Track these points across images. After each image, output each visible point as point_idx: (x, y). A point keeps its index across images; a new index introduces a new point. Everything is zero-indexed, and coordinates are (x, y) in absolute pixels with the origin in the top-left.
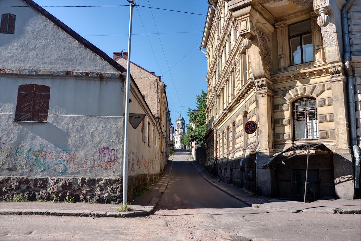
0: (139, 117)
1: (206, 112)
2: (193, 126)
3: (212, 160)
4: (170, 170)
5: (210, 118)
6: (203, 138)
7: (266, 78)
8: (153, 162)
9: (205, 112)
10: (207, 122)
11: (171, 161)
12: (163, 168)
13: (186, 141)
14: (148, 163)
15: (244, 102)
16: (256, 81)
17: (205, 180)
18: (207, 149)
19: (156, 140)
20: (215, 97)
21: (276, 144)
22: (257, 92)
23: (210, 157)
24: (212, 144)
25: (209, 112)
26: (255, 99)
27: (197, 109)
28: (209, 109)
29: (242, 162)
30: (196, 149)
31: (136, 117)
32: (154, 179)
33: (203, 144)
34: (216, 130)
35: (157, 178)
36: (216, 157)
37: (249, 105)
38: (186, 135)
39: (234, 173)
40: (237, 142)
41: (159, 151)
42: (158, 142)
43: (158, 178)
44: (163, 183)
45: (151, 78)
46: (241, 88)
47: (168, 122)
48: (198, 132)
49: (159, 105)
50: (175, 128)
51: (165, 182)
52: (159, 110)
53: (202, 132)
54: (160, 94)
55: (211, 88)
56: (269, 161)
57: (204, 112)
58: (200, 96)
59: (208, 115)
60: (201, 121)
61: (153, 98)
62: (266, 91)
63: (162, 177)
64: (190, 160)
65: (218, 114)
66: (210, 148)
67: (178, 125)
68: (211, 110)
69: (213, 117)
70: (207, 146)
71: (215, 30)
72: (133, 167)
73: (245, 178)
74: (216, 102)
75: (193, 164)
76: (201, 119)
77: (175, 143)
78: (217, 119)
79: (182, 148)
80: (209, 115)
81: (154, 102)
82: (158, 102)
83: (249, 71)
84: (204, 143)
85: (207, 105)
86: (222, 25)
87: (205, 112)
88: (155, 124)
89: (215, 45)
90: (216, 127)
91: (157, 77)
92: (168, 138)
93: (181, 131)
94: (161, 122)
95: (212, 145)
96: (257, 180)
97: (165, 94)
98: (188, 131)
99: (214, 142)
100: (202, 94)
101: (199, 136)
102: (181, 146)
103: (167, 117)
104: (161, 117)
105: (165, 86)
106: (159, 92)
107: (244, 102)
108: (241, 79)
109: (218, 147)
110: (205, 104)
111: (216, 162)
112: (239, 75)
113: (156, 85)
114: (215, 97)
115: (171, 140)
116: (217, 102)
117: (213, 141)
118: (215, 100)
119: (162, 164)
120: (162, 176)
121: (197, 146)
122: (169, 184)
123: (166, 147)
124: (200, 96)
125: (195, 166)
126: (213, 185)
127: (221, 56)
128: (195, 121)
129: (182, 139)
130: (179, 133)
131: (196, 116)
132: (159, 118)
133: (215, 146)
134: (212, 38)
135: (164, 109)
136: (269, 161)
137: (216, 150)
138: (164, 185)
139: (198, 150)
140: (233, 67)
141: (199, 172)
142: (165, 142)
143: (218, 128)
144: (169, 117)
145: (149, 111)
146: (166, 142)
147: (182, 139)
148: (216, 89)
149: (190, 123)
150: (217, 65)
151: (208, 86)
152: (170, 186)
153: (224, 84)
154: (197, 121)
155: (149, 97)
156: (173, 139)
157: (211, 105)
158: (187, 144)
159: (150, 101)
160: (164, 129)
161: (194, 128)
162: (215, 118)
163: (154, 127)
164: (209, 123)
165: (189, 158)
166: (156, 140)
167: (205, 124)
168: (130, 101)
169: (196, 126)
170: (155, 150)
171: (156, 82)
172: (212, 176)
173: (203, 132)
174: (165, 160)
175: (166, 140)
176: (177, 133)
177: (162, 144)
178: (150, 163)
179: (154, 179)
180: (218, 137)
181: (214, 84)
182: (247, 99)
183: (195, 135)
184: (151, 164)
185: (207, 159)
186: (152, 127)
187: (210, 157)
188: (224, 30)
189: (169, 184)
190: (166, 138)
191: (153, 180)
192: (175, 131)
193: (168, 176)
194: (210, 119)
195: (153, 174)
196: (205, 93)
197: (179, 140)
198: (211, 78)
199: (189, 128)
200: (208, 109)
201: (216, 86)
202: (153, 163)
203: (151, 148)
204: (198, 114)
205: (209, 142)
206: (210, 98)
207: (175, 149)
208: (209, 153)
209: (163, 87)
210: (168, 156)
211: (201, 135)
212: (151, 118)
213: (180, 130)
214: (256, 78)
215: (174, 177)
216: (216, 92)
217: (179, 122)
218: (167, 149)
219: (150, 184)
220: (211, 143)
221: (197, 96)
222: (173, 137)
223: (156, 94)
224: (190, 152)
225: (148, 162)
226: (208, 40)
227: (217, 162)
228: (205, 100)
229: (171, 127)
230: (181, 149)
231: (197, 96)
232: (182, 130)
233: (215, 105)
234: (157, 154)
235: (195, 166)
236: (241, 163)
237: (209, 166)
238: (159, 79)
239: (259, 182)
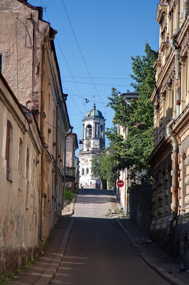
1: (155, 99)
2: (123, 132)
3: (166, 218)
4: (65, 241)
5: (163, 113)
6: (147, 160)
8: (20, 219)
9: (152, 99)
10: (156, 123)
11: (68, 217)
12: (46, 234)
13: (107, 169)
14: (5, 223)
17: (149, 265)
18: (155, 190)
19: (28, 165)
20: (176, 62)
23: (162, 210)
24: (167, 177)
25: (162, 98)
27: (132, 90)
28: (161, 91)
30: (129, 188)
32: (20, 263)
33: (145, 176)
34: (177, 142)
35: (29, 259)
36: (176, 209)
38: (108, 153)
40: (187, 193)
41: (37, 193)
42: (33, 171)
43: (32, 259)
44: (43, 272)
45: (17, 12)
47: (62, 123)
48: (133, 148)
49: (38, 80)
50: (79, 138)
51: (48, 270)
52: (37, 93)
53: (143, 146)
54: (39, 51)
55: (168, 38)
57: (149, 97)
58: (142, 59)
59: (158, 107)
60: (142, 119)
61: (23, 61)
63: (41, 258)
64: (115, 217)
65: (181, 102)
66: (163, 186)
67: (88, 129)
68: (165, 94)
69: (170, 111)
70: (156, 183)
74: (177, 73)
75: (121, 225)
76: (143, 116)
77: (80, 174)
78: (179, 117)
79: (97, 185)
80: (162, 105)
81: (25, 72)
82: (36, 72)
84: (149, 173)
85: (156, 81)
87: (152, 99)
88: (24, 126)
90: (177, 134)
91: (32, 7)
92: (61, 161)
93: (94, 144)
94: (42, 123)
95: (167, 180)
97: (52, 53)
98: (111, 145)
99: (172, 173)
100: (145, 55)
101: (138, 157)
102: (94, 182)
103: (59, 109)
104: (42, 108)
105: (52, 33)
106: (38, 48)
109: (181, 185)
110: (152, 79)
111: (175, 222)
113: (31, 30)
114: (176, 62)
115: (71, 165)
116: (180, 74)
117: (170, 169)
118: (176, 70)
119: (44, 226)
120: (43, 255)
121: (133, 181)
122: (58, 274)
123: (56, 183)
124: (142, 59)
125: (126, 231)
126: (166, 279)
128: (128, 121)
129: (97, 164)
130: (90, 149)
131: (130, 108)
132: (37, 111)
133: (173, 183)
135: (49, 90)
137: (176, 192)
138: (45, 278)
139: (132, 191)
141: (135, 245)
142: (53, 171)
143: (182, 139)
144: (64, 109)
145: (9, 94)
146: (56, 170)
147: (97, 164)
148: (179, 40)
149: (117, 125)
151: (160, 33)
152: (58, 282)
154: (133, 119)
155: (12, 58)
156: (76, 162)
157: (165, 81)
158: (108, 177)
159: (16, 69)
160: (49, 140)
161: (124, 137)
162: (175, 112)
163: (24, 134)
164: (161, 125)
165: (113, 211)
166: (28, 165)
167: (151, 129)
169: (131, 133)
170: (25, 190)
171: (29, 22)
172: (167, 256)
173: (147, 148)
174: (52, 214)
175: (55, 165)
176: (85, 150)
177: (45, 176)
178: (12, 222)
179: (20, 263)
180: (181, 159)
181: (175, 27)
183: (126, 155)
184: (13, 225)
185: (156, 214)
186: (17, 133)
187: (162, 210)
189: (58, 274)
190: (55, 162)
191: (17, 266)
192: (79, 145)
193: (58, 254)
194: (162, 115)
195: (19, 249)
196: (153, 51)
197: (90, 166)
198: (168, 13)
199: (118, 139)
200: (158, 92)
201: (179, 32)
202: (18, 223)
203: (15, 186)
204: (136, 103)
205: (160, 171)
206: (163, 62)
207: (80, 188)
208: (160, 200)
209: (47, 34)
210: (59, 205)
211: (142, 154)
212: (15, 112)
213: (92, 141)
215: (71, 257)
216: (178, 48)
217: (92, 123)
218: (58, 187)
219: (9, 276)
220: (164, 174)
221: (133, 59)
222: (74, 158)
223: (31, 51)
224: (115, 197)
225: (6, 219)
227: (177, 222)
228: (152, 69)
229: (68, 135)
230: (93, 187)
231: (133, 59)
232: (98, 142)
233: (175, 82)
234: (31, 200)
235: (126, 231)
237: (160, 230)
238: (36, 13)
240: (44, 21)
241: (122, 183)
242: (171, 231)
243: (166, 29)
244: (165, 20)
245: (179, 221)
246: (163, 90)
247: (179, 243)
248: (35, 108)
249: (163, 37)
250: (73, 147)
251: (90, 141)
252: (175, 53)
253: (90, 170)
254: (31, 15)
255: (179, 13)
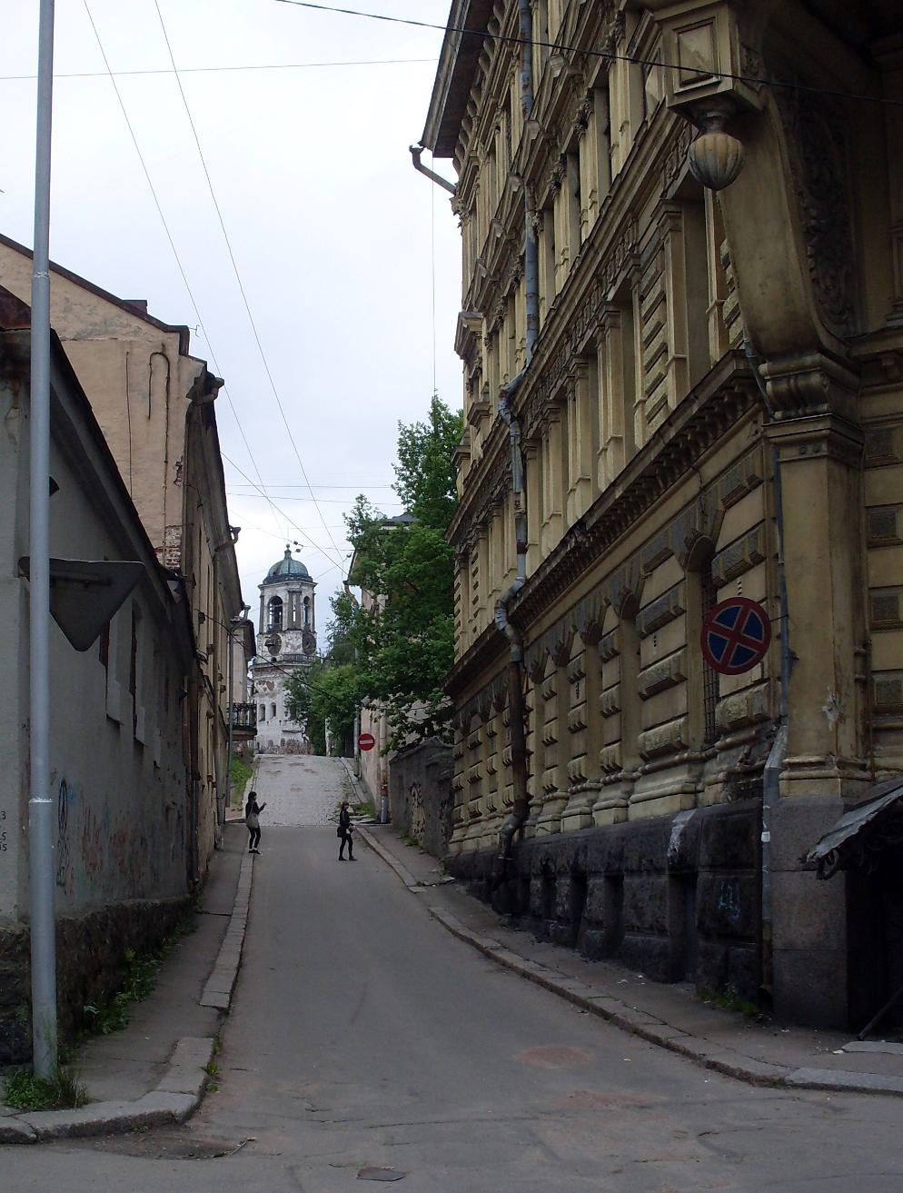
0: (109, 583)
7: (824, 351)
15: (692, 487)
16: (763, 368)
20: (516, 453)
21: (878, 730)
22: (771, 433)
26: (758, 474)
29: (683, 835)
31: (87, 584)
37: (721, 508)
39: (634, 895)
46: (673, 404)
56: (842, 829)
62: (820, 426)
66: (481, 749)
71: (510, 55)
72: (63, 865)
73: (701, 923)
83: (720, 305)
86: (555, 30)
89: (509, 138)
92: (224, 689)
96: (766, 937)
107: (692, 487)
108: (672, 353)
111: (516, 836)
112: (659, 326)
114: (516, 453)
127: (549, 208)
134: (491, 101)
136: (842, 829)
140: (626, 282)
143: (533, 635)
150: (522, 258)
153: (572, 378)
168: (53, 487)
182: (710, 469)
184: (147, 845)
188: (567, 60)
197: (282, 697)
198: (484, 335)
205: (474, 712)
214: (762, 354)
226: (463, 114)
236: (675, 838)
237: (476, 853)
238: (174, 340)
239: (777, 943)
240: (193, 358)
241: (371, 742)
242: (508, 854)
243: (482, 373)
244: (478, 353)
245: (526, 829)
246: (478, 517)
247: (527, 882)
248: (173, 564)
249: (472, 391)
250: (245, 656)
251: (279, 638)
252: (512, 430)
253: (281, 710)
254: (163, 345)
255: (513, 337)
